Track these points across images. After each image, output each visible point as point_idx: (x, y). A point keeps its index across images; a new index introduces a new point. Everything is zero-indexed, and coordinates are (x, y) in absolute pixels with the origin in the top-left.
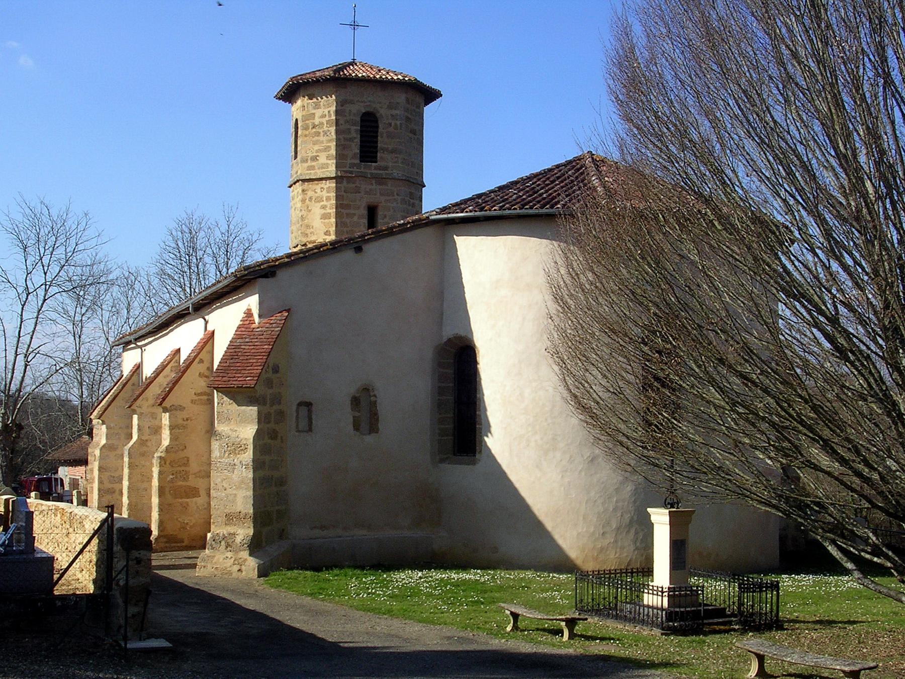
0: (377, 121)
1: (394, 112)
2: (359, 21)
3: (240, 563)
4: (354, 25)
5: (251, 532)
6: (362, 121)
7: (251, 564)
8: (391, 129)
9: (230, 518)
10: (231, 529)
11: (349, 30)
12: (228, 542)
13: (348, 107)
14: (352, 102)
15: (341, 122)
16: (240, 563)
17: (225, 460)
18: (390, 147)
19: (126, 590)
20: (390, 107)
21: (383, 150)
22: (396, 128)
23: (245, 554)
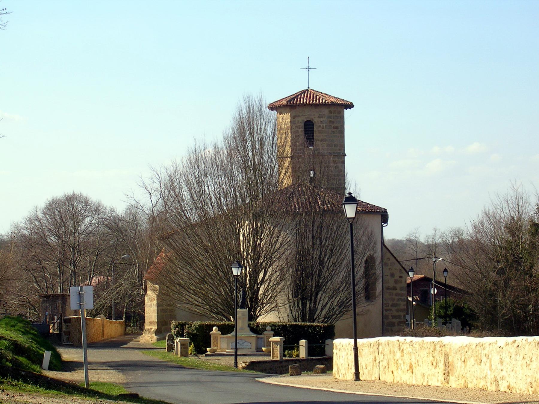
0: (313, 125)
1: (322, 119)
2: (311, 66)
3: (152, 338)
4: (308, 69)
5: (156, 327)
6: (305, 125)
7: (155, 337)
8: (320, 129)
9: (151, 323)
10: (151, 327)
11: (306, 71)
12: (149, 331)
13: (297, 119)
14: (299, 116)
15: (294, 127)
16: (152, 338)
17: (149, 303)
18: (320, 138)
19: (65, 332)
20: (319, 117)
21: (318, 140)
22: (323, 128)
23: (154, 335)
